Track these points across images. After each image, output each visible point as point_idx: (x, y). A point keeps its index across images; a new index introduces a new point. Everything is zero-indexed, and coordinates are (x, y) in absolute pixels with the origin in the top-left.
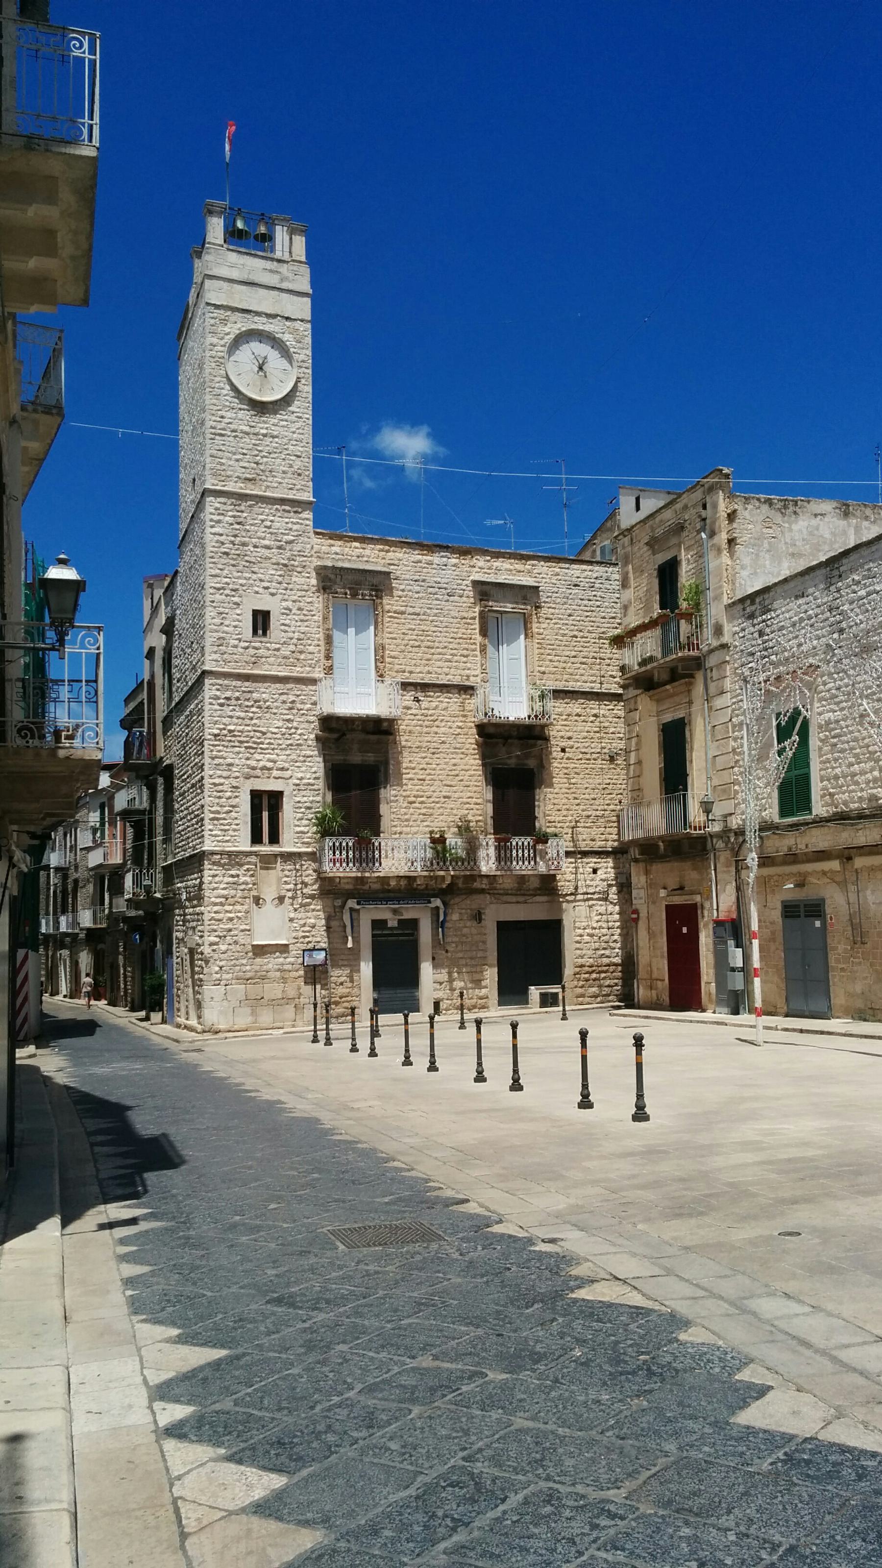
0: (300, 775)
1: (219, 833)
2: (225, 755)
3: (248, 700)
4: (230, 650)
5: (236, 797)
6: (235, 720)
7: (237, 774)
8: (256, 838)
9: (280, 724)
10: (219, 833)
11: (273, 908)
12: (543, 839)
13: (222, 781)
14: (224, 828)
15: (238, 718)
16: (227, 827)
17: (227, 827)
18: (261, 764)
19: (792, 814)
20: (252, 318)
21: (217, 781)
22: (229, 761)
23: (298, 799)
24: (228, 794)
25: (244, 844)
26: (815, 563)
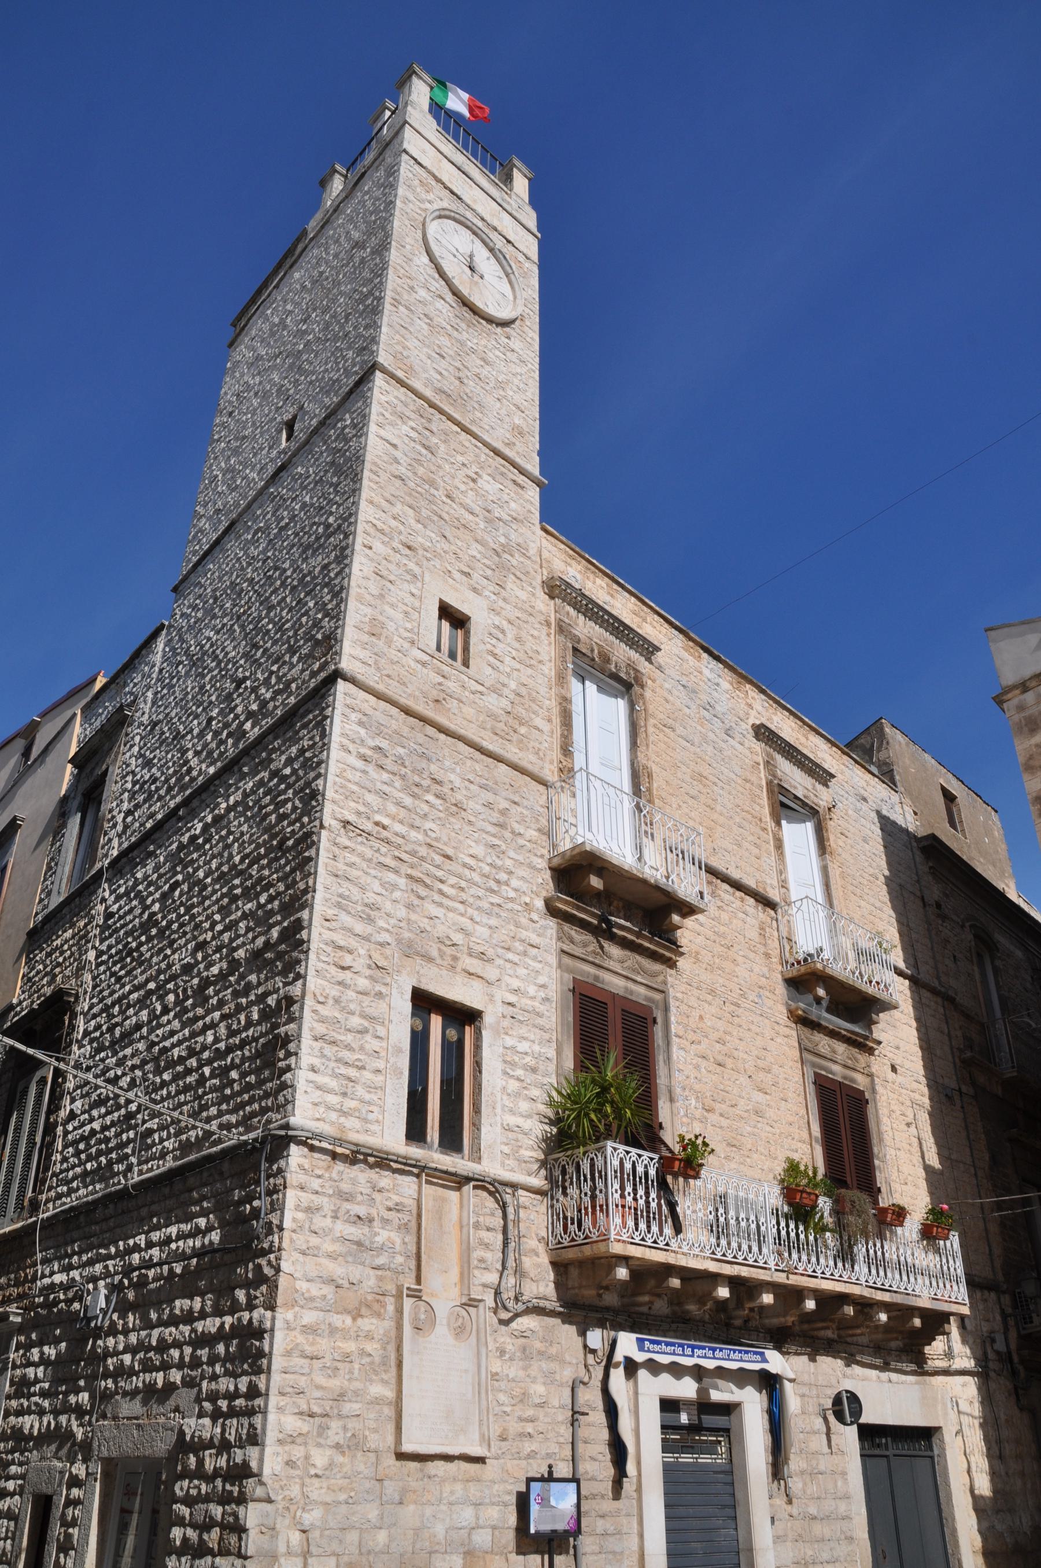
0: (515, 983)
1: (333, 1084)
2: (364, 880)
3: (420, 772)
4: (393, 654)
5: (380, 995)
6: (392, 808)
7: (385, 937)
8: (416, 1132)
9: (479, 850)
10: (333, 1084)
11: (450, 1340)
12: (687, 1163)
13: (353, 943)
14: (344, 1076)
15: (398, 804)
16: (352, 1072)
17: (352, 1072)
18: (441, 930)
19: (32, 1058)
20: (455, 254)
21: (340, 939)
22: (371, 897)
23: (509, 1042)
24: (363, 983)
25: (391, 1136)
26: (673, 1019)
